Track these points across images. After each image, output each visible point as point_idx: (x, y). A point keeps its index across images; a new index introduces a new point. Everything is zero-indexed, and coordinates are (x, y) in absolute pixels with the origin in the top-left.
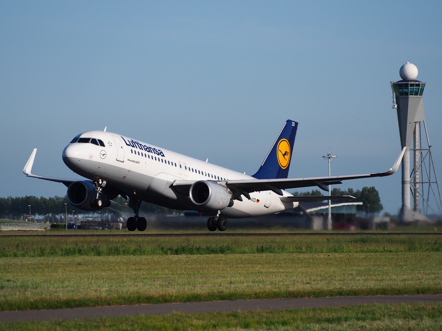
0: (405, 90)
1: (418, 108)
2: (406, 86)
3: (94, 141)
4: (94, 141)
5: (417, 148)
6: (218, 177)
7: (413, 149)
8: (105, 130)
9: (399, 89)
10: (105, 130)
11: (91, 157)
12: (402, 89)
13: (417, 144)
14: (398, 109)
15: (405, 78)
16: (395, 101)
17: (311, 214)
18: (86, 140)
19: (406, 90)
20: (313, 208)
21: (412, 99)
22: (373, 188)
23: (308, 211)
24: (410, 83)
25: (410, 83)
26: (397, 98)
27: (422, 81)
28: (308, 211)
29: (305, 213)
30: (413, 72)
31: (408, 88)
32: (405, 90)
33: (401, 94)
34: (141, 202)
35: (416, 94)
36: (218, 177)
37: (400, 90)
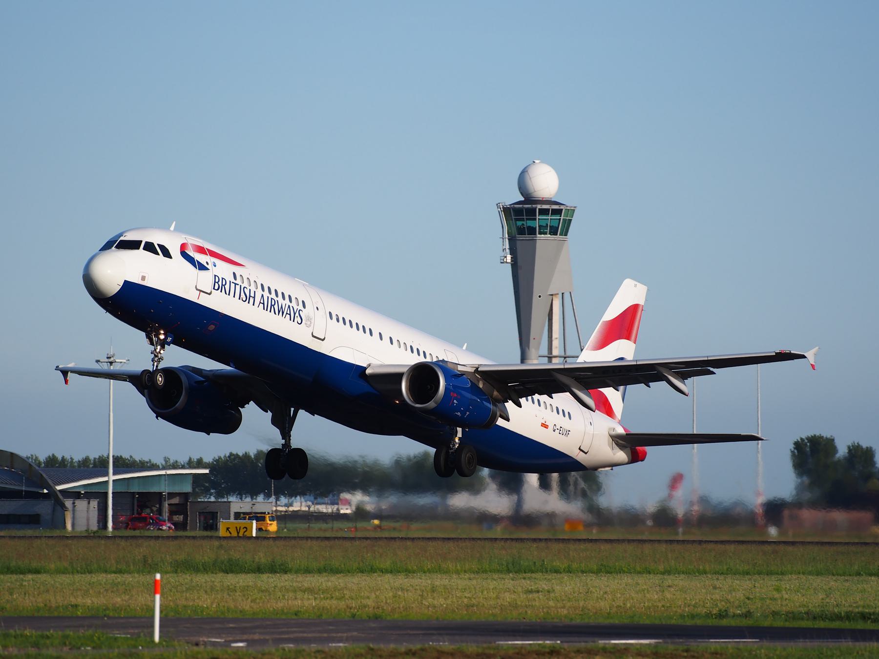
0: (529, 221)
1: (564, 263)
2: (531, 213)
3: (150, 247)
4: (150, 247)
5: (555, 352)
6: (533, 402)
7: (546, 353)
8: (172, 228)
9: (517, 220)
10: (172, 228)
11: (143, 278)
12: (523, 220)
13: (555, 343)
14: (515, 265)
15: (529, 199)
16: (508, 247)
17: (75, 495)
18: (134, 245)
19: (530, 223)
20: (68, 483)
21: (543, 241)
22: (798, 445)
23: (59, 488)
24: (539, 206)
25: (539, 206)
26: (512, 240)
27: (567, 201)
28: (59, 488)
29: (53, 494)
30: (546, 183)
31: (535, 219)
32: (529, 221)
33: (521, 231)
34: (194, 489)
35: (554, 231)
36: (533, 402)
37: (519, 223)
